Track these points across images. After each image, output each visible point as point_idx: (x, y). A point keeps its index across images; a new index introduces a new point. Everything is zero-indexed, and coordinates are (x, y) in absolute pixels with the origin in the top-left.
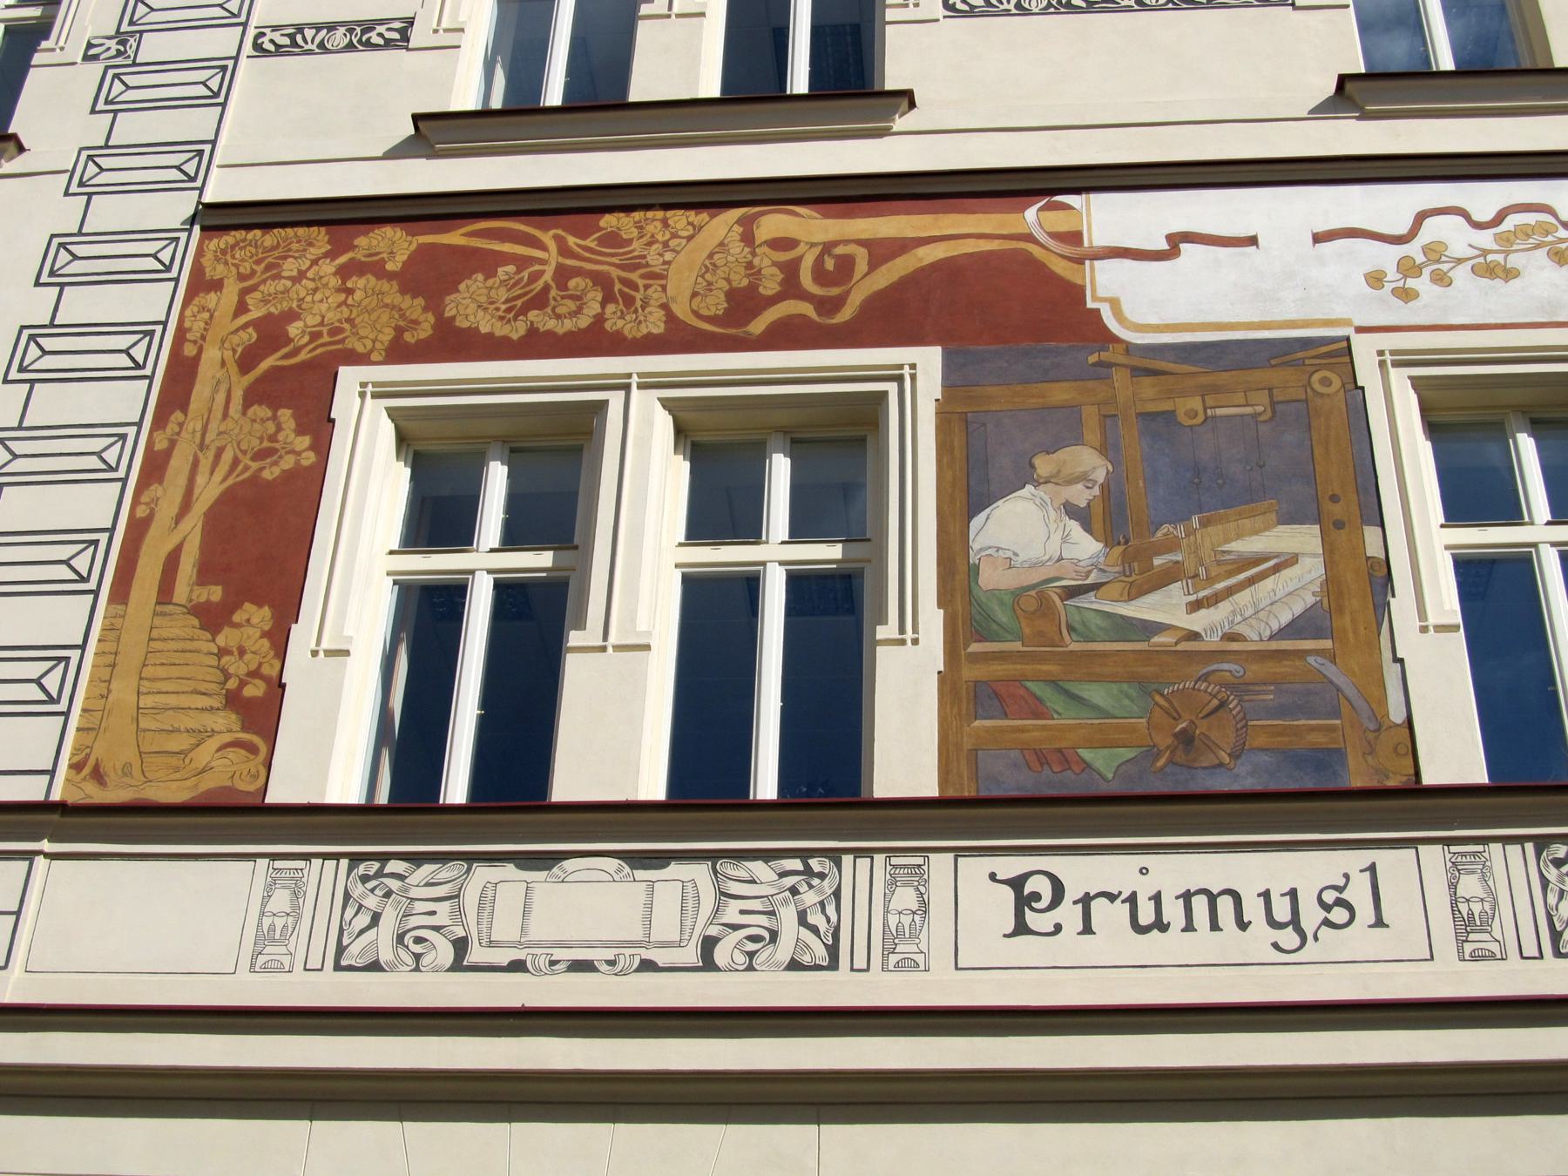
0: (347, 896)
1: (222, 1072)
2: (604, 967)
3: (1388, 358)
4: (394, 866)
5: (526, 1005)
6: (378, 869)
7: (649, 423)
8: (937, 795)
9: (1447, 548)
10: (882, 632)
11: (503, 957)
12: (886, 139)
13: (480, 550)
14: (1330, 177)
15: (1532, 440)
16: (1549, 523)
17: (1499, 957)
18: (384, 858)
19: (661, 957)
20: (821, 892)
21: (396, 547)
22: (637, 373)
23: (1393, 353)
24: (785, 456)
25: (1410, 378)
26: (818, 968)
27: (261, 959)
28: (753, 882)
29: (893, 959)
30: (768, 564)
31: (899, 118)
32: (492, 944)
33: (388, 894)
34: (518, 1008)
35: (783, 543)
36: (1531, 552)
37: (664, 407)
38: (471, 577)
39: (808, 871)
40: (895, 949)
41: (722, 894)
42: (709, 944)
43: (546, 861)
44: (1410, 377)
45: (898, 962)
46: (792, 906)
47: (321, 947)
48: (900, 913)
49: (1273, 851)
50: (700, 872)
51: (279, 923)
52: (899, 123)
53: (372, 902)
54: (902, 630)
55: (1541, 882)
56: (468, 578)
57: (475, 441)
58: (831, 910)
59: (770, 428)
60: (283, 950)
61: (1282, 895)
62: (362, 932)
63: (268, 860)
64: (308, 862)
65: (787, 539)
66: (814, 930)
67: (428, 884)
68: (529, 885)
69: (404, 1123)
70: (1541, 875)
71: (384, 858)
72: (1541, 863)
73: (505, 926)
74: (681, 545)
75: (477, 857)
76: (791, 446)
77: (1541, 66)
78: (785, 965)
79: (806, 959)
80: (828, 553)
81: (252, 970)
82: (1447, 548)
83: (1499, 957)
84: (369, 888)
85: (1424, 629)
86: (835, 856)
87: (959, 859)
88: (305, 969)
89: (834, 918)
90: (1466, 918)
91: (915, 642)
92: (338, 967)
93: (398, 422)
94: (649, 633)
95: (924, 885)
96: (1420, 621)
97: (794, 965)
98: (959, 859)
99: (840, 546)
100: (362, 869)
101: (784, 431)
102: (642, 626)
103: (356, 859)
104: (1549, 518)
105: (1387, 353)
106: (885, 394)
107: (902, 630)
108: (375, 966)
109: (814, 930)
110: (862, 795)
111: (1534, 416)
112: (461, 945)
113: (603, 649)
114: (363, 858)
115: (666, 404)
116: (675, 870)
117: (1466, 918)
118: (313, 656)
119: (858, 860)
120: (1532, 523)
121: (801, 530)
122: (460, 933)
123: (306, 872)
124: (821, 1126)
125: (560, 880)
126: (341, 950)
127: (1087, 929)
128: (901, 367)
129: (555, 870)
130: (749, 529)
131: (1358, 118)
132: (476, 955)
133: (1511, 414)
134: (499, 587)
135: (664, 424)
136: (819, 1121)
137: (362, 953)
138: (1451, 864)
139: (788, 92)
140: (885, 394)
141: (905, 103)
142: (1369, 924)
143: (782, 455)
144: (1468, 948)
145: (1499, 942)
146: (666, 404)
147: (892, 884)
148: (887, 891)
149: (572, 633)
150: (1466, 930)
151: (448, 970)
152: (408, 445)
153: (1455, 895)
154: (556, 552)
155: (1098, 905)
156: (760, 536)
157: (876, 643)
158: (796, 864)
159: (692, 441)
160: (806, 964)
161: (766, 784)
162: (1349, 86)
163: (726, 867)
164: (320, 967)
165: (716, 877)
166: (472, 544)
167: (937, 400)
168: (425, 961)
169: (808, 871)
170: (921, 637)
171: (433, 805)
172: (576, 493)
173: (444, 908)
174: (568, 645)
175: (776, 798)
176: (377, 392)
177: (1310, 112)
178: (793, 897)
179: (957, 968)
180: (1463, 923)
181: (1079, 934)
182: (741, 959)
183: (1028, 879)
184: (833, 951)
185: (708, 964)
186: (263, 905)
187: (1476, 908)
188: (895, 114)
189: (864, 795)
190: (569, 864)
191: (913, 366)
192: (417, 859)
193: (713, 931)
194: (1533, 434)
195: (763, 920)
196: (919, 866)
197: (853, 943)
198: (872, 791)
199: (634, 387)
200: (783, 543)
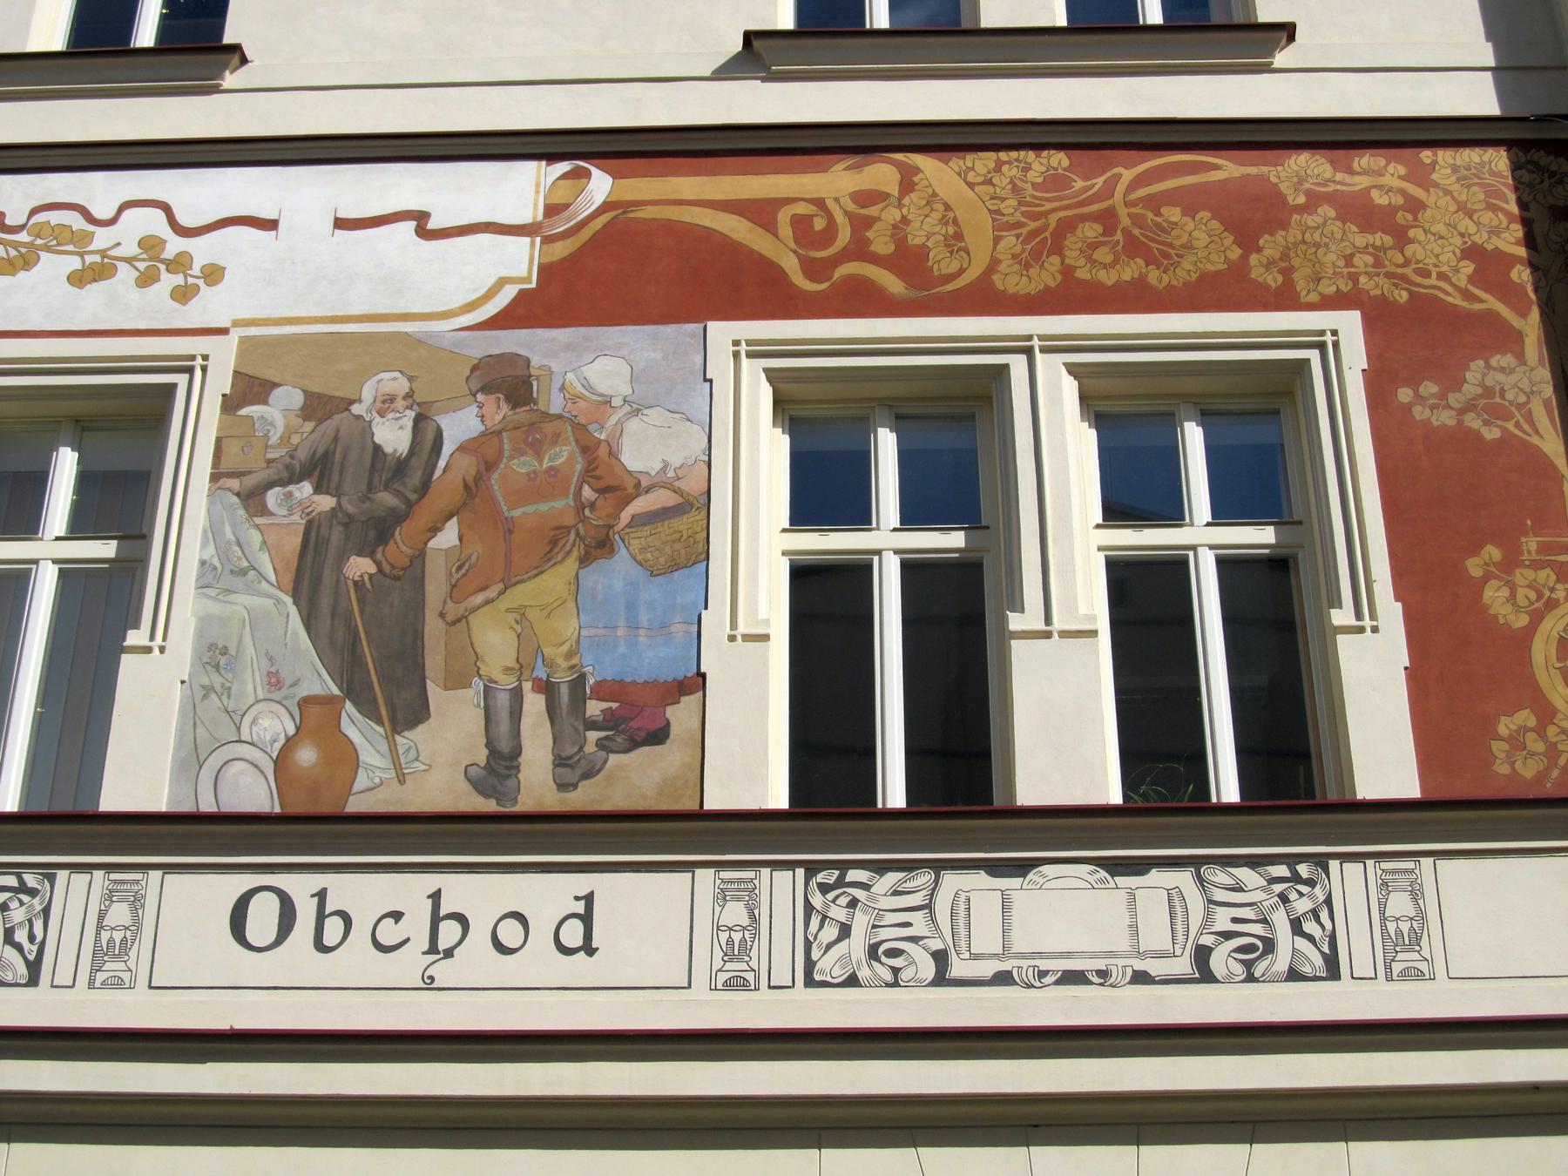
0: (809, 908)
1: (48, 1097)
2: (1096, 979)
3: (743, 348)
4: (854, 875)
7: (1056, 387)
11: (987, 969)
13: (45, 539)
15: (1200, 429)
16: (1208, 524)
17: (1428, 977)
18: (844, 866)
19: (1155, 968)
20: (1312, 897)
21: (787, 526)
22: (1037, 335)
23: (748, 343)
24: (72, 450)
25: (765, 370)
26: (1316, 979)
27: (100, 977)
28: (1241, 890)
32: (976, 957)
33: (853, 903)
34: (226, 1030)
35: (895, 530)
36: (1188, 555)
37: (1070, 373)
38: (34, 567)
39: (1296, 878)
40: (1395, 957)
41: (1211, 902)
42: (1202, 955)
43: (1021, 868)
45: (726, 981)
47: (783, 960)
50: (1183, 879)
51: (118, 936)
53: (839, 913)
54: (152, 638)
58: (1324, 915)
60: (122, 966)
62: (829, 947)
65: (898, 526)
67: (896, 893)
68: (1170, 892)
69: (1349, 1143)
70: (807, 900)
71: (844, 866)
72: (47, 899)
73: (986, 936)
74: (784, 530)
75: (1156, 862)
77: (1238, 19)
79: (1307, 970)
80: (1259, 536)
81: (1389, 978)
82: (784, 553)
83: (1428, 977)
84: (830, 899)
86: (1321, 861)
88: (52, 986)
89: (1328, 926)
90: (1394, 939)
91: (162, 650)
92: (810, 982)
93: (776, 385)
94: (767, 622)
95: (1419, 890)
96: (731, 630)
97: (1294, 975)
99: (114, 543)
100: (820, 877)
102: (762, 615)
103: (812, 869)
105: (743, 343)
107: (152, 638)
108: (852, 981)
111: (1205, 407)
112: (940, 958)
113: (1047, 635)
115: (1072, 369)
116: (1156, 876)
117: (1394, 939)
119: (774, 873)
120: (1192, 525)
121: (911, 517)
122: (936, 945)
123: (1417, 871)
124: (1140, 1147)
125: (1038, 887)
128: (193, 358)
129: (1030, 876)
130: (859, 514)
131: (764, 80)
132: (958, 969)
133: (1181, 405)
134: (905, 566)
135: (1070, 387)
136: (1346, 1138)
138: (719, 891)
139: (868, 26)
142: (423, 951)
143: (69, 449)
144: (1397, 968)
145: (755, 971)
146: (1072, 369)
148: (1380, 896)
150: (1394, 949)
151: (930, 985)
152: (783, 409)
153: (1384, 914)
154: (121, 541)
157: (1006, 636)
158: (1281, 870)
159: (790, 416)
161: (894, 791)
162: (756, 43)
163: (1209, 872)
164: (71, 984)
165: (1203, 886)
166: (37, 533)
168: (905, 975)
169: (1296, 878)
170: (168, 644)
171: (871, 810)
173: (918, 918)
175: (787, 807)
180: (1392, 944)
181: (424, 953)
182: (1239, 969)
183: (251, 897)
184: (34, 968)
185: (1206, 975)
187: (1405, 927)
189: (998, 801)
190: (1046, 869)
191: (205, 358)
192: (881, 868)
193: (1207, 940)
194: (1201, 423)
195: (1258, 929)
197: (1358, 949)
199: (1037, 350)
200: (895, 530)
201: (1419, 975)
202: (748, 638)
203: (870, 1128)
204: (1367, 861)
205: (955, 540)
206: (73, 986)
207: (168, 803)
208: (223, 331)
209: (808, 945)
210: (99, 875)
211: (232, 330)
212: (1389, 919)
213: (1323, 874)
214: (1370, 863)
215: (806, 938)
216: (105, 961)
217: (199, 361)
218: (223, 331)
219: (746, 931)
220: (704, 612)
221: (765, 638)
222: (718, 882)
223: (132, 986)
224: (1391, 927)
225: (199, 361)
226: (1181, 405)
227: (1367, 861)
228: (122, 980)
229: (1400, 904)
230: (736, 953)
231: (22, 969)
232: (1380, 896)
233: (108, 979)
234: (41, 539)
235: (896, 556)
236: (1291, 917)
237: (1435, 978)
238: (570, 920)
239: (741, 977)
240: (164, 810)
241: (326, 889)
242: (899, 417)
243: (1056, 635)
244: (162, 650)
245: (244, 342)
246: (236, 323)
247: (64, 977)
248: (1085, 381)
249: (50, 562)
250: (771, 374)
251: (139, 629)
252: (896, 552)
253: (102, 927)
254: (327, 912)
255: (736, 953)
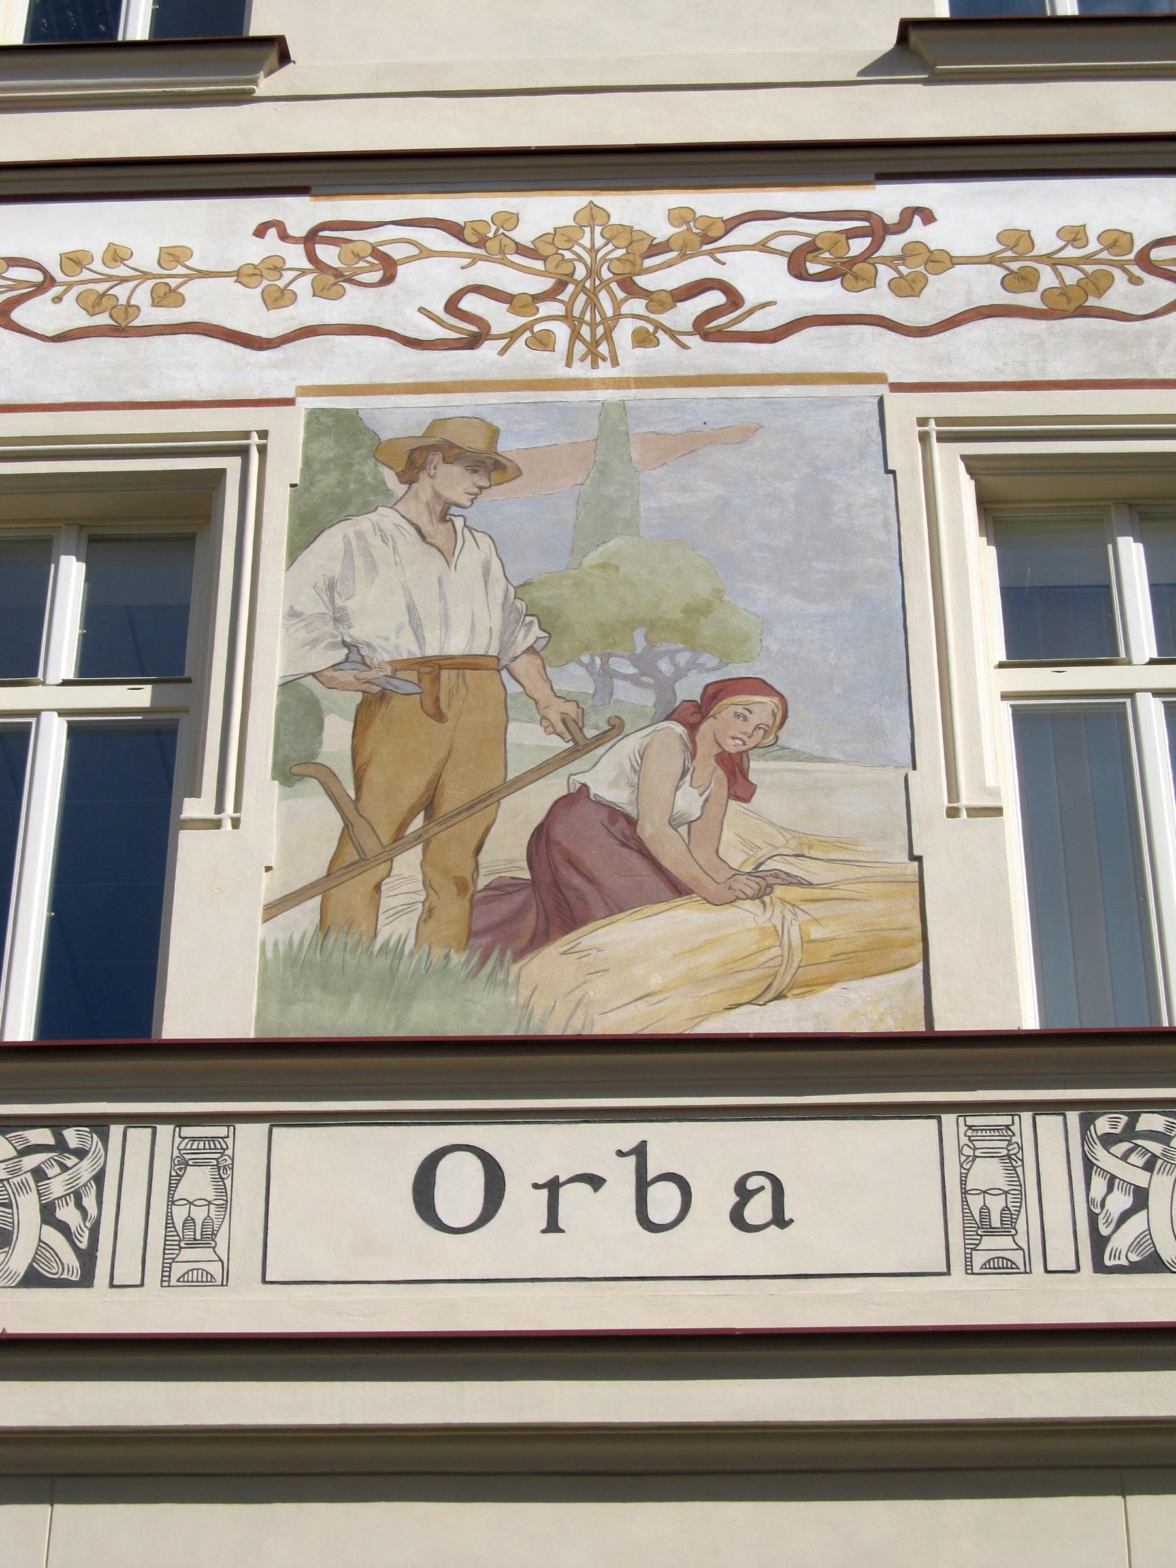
0: (1089, 1166)
5: (9, 1331)
6: (1126, 1125)
7: (953, 482)
8: (1038, 1028)
9: (1005, 696)
10: (192, 808)
12: (246, 108)
13: (48, 682)
14: (234, 186)
21: (1003, 658)
23: (940, 421)
24: (78, 561)
25: (964, 458)
29: (979, 1259)
30: (1138, 694)
31: (267, 75)
36: (1124, 703)
38: (33, 720)
39: (61, 1146)
44: (963, 457)
46: (34, 1195)
48: (985, 1192)
49: (579, 1122)
52: (265, 85)
54: (220, 807)
55: (1084, 1165)
56: (30, 723)
57: (30, 525)
59: (1109, 499)
61: (536, 1186)
63: (172, 1127)
64: (1016, 1118)
66: (63, 1228)
74: (1001, 665)
76: (88, 547)
78: (19, 1279)
79: (51, 1271)
81: (969, 1270)
82: (1005, 696)
85: (953, 813)
87: (1037, 1117)
90: (181, 1235)
91: (236, 823)
96: (949, 802)
97: (33, 1279)
98: (1037, 1117)
99: (148, 688)
100: (1103, 1125)
101: (79, 524)
103: (1090, 1111)
104: (1003, 658)
106: (222, 472)
107: (220, 807)
109: (63, 1228)
110: (153, 1037)
111: (94, 531)
114: (33, 1123)
117: (181, 1235)
118: (949, 816)
119: (275, 1130)
126: (1099, 1243)
127: (553, 1226)
128: (247, 435)
131: (925, 82)
133: (1112, 507)
134: (74, 732)
135: (967, 488)
137: (1136, 1245)
139: (120, 38)
140: (222, 472)
141: (273, 56)
143: (74, 558)
144: (979, 1259)
147: (180, 1166)
149: (188, 802)
151: (20, 1285)
155: (570, 1195)
156: (1116, 652)
158: (43, 1136)
160: (50, 1276)
162: (914, 36)
166: (36, 674)
167: (293, 486)
169: (61, 1146)
170: (243, 816)
172: (187, 608)
174: (182, 816)
176: (944, 432)
177: (860, 74)
178: (37, 1182)
179: (264, 1281)
180: (177, 1238)
181: (543, 1231)
184: (88, 1258)
186: (172, 1188)
187: (199, 1214)
188: (258, 71)
191: (263, 434)
196: (1007, 1127)
198: (161, 1034)
201: (207, 1280)
202: (974, 812)
203: (546, 1474)
204: (943, 1116)
205: (138, 697)
206: (142, 1285)
207: (256, 1031)
208: (290, 402)
209: (1093, 1218)
210: (165, 1131)
211: (299, 400)
212: (970, 1192)
213: (100, 1143)
214: (949, 1119)
215: (1090, 1211)
216: (981, 1236)
217: (255, 440)
218: (290, 402)
219: (1008, 1195)
220: (911, 773)
221: (997, 811)
222: (963, 1129)
223: (225, 1283)
224: (975, 1203)
225: (255, 440)
226: (1112, 507)
227: (943, 1116)
228: (212, 1276)
229: (198, 1183)
230: (198, 1237)
231: (71, 1259)
232: (174, 1173)
233: (187, 1272)
234: (43, 683)
235: (1158, 699)
236: (1118, 1180)
237: (1031, 1272)
238: (658, 1183)
239: (1003, 1258)
240: (252, 1037)
241: (645, 1142)
242: (93, 540)
243: (964, 813)
244: (236, 823)
245: (314, 416)
246: (305, 391)
247: (127, 1271)
248: (990, 480)
249: (56, 714)
250: (973, 465)
251: (199, 797)
252: (62, 713)
253: (173, 1203)
254: (650, 1177)
255: (198, 1237)
